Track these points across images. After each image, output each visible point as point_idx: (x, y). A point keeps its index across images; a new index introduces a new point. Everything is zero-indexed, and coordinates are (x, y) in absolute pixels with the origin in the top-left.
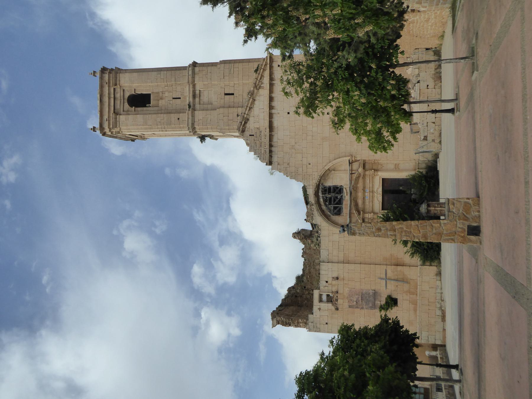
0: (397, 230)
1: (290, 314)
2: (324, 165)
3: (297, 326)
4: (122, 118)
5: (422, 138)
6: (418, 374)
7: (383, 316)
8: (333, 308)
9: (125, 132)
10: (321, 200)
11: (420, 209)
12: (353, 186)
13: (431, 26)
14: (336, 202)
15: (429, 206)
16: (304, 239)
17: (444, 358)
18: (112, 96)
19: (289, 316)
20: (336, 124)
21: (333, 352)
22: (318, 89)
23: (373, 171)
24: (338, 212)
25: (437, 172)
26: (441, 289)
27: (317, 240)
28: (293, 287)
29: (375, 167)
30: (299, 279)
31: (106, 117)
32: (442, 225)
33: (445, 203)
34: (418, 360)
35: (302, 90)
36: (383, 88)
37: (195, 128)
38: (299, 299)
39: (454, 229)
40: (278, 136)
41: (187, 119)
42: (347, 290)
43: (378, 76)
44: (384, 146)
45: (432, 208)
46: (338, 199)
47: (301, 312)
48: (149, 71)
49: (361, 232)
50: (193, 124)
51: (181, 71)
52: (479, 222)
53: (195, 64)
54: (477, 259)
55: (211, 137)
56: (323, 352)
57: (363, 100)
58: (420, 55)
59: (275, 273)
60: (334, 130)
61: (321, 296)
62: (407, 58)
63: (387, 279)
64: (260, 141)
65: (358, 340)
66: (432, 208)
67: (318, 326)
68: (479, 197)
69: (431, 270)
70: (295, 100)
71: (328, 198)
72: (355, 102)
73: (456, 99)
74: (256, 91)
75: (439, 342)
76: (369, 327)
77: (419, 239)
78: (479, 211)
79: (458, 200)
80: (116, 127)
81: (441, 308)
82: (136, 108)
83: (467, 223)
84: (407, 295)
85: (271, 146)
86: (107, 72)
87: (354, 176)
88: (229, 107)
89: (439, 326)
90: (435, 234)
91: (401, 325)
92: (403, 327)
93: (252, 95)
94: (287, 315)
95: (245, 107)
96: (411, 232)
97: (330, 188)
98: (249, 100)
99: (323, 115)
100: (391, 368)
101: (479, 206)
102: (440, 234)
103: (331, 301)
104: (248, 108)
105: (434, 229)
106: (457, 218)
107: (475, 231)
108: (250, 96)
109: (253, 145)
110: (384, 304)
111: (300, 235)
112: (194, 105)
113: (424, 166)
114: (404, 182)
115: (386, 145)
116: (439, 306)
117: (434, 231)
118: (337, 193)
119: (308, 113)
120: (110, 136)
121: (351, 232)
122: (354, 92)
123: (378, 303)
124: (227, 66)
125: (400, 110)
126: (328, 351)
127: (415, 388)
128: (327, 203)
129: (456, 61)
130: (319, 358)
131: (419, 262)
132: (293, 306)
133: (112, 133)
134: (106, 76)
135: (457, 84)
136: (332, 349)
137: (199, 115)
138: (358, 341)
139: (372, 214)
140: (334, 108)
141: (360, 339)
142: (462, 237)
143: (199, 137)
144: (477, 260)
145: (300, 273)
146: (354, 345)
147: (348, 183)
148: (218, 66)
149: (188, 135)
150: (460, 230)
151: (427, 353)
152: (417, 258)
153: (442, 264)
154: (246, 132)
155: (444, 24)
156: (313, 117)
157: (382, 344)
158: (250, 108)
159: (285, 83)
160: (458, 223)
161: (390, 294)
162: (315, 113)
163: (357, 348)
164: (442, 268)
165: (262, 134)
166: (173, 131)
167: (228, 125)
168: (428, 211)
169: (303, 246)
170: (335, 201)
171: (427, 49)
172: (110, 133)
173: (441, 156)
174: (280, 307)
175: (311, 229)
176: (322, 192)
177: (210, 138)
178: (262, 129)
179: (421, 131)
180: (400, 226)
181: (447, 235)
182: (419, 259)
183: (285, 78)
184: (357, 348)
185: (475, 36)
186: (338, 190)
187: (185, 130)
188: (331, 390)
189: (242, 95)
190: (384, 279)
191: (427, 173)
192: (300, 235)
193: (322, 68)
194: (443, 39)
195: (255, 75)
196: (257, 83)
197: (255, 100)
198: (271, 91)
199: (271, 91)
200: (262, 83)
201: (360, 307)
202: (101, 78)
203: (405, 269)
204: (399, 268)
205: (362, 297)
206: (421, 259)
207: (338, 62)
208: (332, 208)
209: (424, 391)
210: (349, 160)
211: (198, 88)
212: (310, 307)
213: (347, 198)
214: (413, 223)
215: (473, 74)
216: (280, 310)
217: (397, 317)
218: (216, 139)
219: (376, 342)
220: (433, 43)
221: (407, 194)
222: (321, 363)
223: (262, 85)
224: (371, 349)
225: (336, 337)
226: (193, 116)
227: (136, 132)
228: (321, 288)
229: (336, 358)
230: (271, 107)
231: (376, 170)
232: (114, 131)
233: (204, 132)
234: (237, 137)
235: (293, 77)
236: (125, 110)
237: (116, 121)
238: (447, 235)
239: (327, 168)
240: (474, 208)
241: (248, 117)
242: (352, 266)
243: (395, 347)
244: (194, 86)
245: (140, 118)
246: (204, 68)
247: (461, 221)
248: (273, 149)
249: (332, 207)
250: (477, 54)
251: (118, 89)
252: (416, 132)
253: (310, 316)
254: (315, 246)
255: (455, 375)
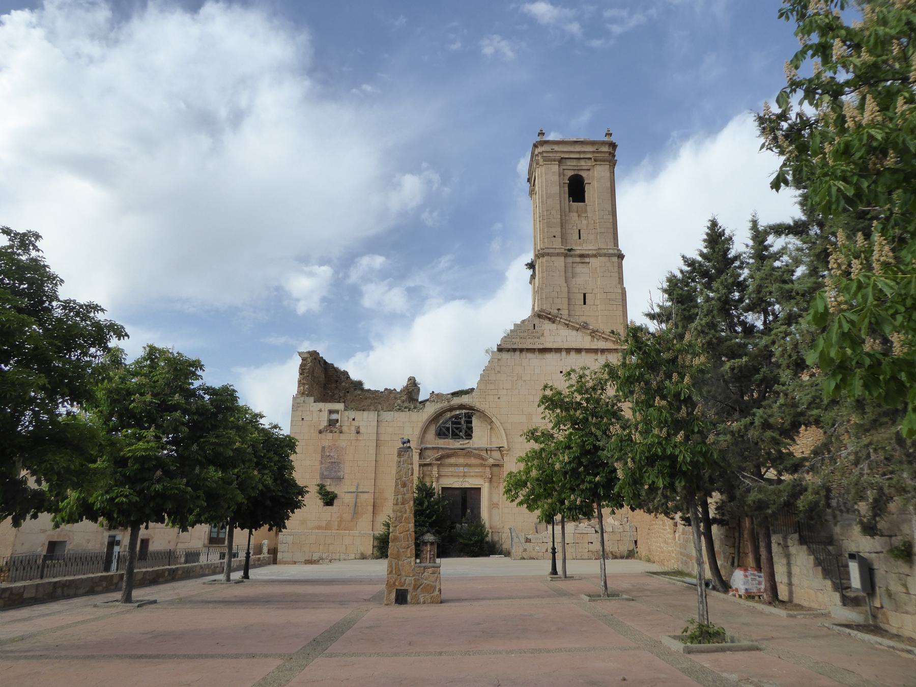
0: (403, 506)
1: (315, 375)
2: (498, 416)
3: (299, 382)
4: (555, 168)
5: (529, 537)
6: (237, 531)
7: (307, 489)
8: (321, 427)
9: (538, 171)
10: (458, 412)
11: (429, 534)
12: (471, 452)
13: (660, 547)
14: (455, 430)
15: (432, 544)
16: (406, 391)
17: (259, 563)
18: (582, 156)
19: (312, 372)
20: (533, 434)
21: (263, 429)
22: (572, 412)
23: (490, 476)
24: (441, 434)
25: (487, 555)
26: (345, 560)
27: (405, 408)
28: (348, 377)
29: (494, 478)
30: (359, 384)
31: (556, 148)
32: (409, 560)
33: (435, 563)
34: (253, 530)
35: (572, 393)
36: (573, 490)
37: (543, 256)
38: (334, 385)
39: (403, 573)
40: (534, 360)
41: (554, 247)
42: (343, 444)
43: (586, 484)
44: (510, 490)
45: (429, 548)
46: (458, 433)
47: (317, 387)
48: (612, 201)
49: (402, 463)
50: (548, 254)
51: (612, 240)
52: (411, 603)
53: (621, 257)
54: (369, 600)
55: (533, 277)
56: (264, 416)
57: (557, 466)
58: (629, 533)
59: (373, 355)
60: (525, 431)
61: (337, 412)
62: (627, 518)
63: (357, 493)
64: (528, 337)
65: (277, 459)
66: (429, 548)
67: (300, 409)
68: (441, 602)
69: (368, 547)
70: (562, 385)
71: (459, 420)
72: (557, 457)
73: (566, 577)
74: (589, 332)
75: (279, 556)
76: (294, 472)
77: (392, 532)
78: (424, 603)
79: (438, 579)
80: (544, 161)
81: (322, 559)
82: (567, 185)
83: (410, 589)
84: (338, 518)
85: (521, 350)
86: (611, 150)
87: (484, 454)
88: (569, 299)
89: (299, 556)
90: (398, 551)
91: (295, 510)
92: (293, 512)
93: (585, 327)
94: (313, 371)
95: (569, 319)
96: (401, 523)
97: (471, 422)
98: (578, 324)
99: (542, 418)
100: (240, 498)
101: (430, 603)
102: (398, 557)
103: (330, 425)
104: (567, 322)
105: (404, 550)
106: (417, 577)
107: (401, 598)
108: (583, 325)
109: (523, 328)
110: (326, 489)
111: (412, 387)
112: (571, 256)
113: (496, 538)
114: (477, 515)
115: (513, 493)
116: (324, 556)
117: (401, 550)
118: (466, 432)
119: (545, 399)
120: (533, 153)
121: (402, 451)
122: (567, 455)
123: (327, 483)
124: (619, 297)
125: (553, 510)
126: (265, 423)
127: (708, 505)
128: (454, 419)
129: (603, 576)
130: (257, 411)
131: (378, 532)
132: (325, 377)
133: (537, 155)
134: (605, 149)
135: (585, 578)
136: (267, 427)
137: (560, 262)
138: (276, 458)
139: (437, 475)
140: (551, 432)
141: (279, 461)
142: (394, 583)
143: (532, 262)
144: (369, 600)
145: (366, 386)
146: (271, 454)
147: (476, 446)
148: (619, 286)
149: (535, 248)
150: (403, 580)
151: (266, 542)
152: (383, 530)
153: (375, 560)
154: (538, 319)
155: (662, 563)
156: (539, 406)
157: (272, 487)
158: (567, 325)
159: (581, 373)
160: (410, 578)
161: (338, 497)
162: (545, 409)
163: (268, 458)
164: (370, 561)
165: (536, 340)
166: (540, 230)
167: (546, 298)
168: (425, 543)
169: (398, 390)
170: (457, 428)
171: (636, 542)
172: (536, 152)
173: (507, 559)
174: (323, 362)
175: (420, 400)
176: (468, 413)
177: (531, 275)
178: (542, 339)
179: (537, 536)
180: (408, 510)
181: (397, 564)
182: (381, 533)
183: (587, 372)
184: (268, 458)
185: (631, 597)
186: (470, 433)
187: (540, 244)
188: (215, 427)
189: (585, 314)
190: (357, 490)
191: (487, 542)
192: (412, 387)
193: (597, 418)
194: (646, 561)
195: (608, 331)
196: (598, 334)
197: (577, 330)
198: (588, 351)
199: (588, 351)
200: (598, 340)
201: (323, 461)
202: (603, 143)
203: (369, 515)
204: (371, 509)
205: (335, 462)
206: (381, 535)
207: (602, 437)
208: (447, 426)
209: (222, 538)
210: (503, 447)
211: (592, 260)
212: (324, 397)
213: (457, 444)
214: (411, 526)
215: (587, 595)
216: (319, 361)
217: (305, 505)
218: (530, 283)
219: (275, 480)
220: (642, 550)
221: (462, 518)
222: (250, 414)
223: (595, 339)
224: (267, 474)
225: (282, 432)
226: (558, 255)
227: (538, 184)
228: (347, 413)
229: (256, 433)
230: (568, 351)
231: (491, 480)
232: (539, 158)
233: (539, 268)
234: (533, 309)
235: (588, 382)
236: (565, 171)
237: (551, 161)
238: (397, 564)
239: (494, 419)
240: (428, 596)
241: (557, 322)
242: (372, 451)
243: (268, 503)
244: (595, 256)
245: (555, 189)
246: (616, 269)
247: (413, 582)
248: (518, 353)
249: (449, 425)
250: (609, 600)
251: (590, 163)
252: (536, 528)
253: (312, 399)
254: (399, 405)
255: (237, 575)
